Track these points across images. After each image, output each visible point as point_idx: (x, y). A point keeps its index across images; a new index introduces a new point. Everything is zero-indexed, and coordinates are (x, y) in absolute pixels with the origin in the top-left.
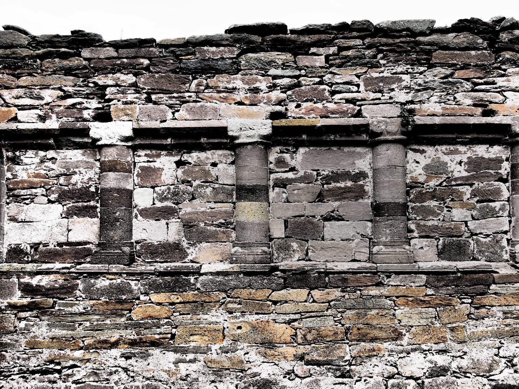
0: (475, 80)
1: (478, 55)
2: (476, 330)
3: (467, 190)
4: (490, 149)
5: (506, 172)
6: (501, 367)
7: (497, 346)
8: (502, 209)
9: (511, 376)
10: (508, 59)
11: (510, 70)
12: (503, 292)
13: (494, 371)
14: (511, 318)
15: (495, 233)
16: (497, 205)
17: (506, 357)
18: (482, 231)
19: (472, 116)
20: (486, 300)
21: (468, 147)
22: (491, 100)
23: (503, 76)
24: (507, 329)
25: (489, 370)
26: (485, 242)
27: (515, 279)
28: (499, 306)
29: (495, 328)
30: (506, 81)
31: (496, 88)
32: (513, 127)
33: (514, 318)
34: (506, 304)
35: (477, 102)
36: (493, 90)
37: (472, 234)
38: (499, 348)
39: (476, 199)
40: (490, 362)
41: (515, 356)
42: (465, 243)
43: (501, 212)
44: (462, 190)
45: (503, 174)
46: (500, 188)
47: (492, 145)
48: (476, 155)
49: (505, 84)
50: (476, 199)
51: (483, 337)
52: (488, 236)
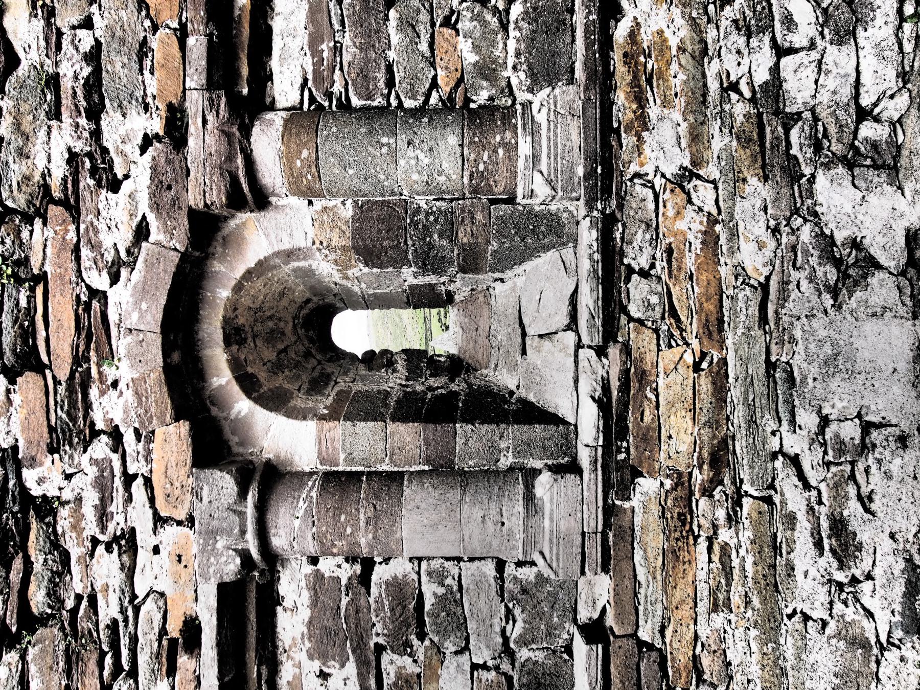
0: (106, 673)
1: (40, 671)
2: (758, 681)
3: (392, 662)
4: (287, 603)
5: (346, 566)
6: (857, 617)
7: (800, 627)
8: (439, 577)
9: (880, 592)
10: (48, 595)
11: (78, 586)
12: (660, 613)
13: (867, 635)
14: (728, 592)
15: (502, 596)
16: (430, 590)
17: (831, 603)
18: (497, 629)
19: (198, 678)
20: (680, 656)
21: (283, 658)
22: (156, 630)
23: (93, 600)
24: (756, 601)
25: (864, 647)
26: (525, 622)
27: (627, 582)
28: (695, 624)
29: (753, 633)
30: (106, 597)
31: (126, 620)
32: (227, 579)
33: (729, 585)
34: (692, 604)
35: (164, 669)
36: (131, 628)
37: (508, 652)
38: (806, 618)
39: (416, 642)
40: (842, 644)
41: (830, 581)
42: (528, 674)
43: (449, 581)
44: (392, 675)
45: (351, 572)
46: (387, 583)
47: (277, 600)
48: (302, 638)
49: (114, 598)
50: (416, 642)
51: (776, 664)
52: (509, 613)
